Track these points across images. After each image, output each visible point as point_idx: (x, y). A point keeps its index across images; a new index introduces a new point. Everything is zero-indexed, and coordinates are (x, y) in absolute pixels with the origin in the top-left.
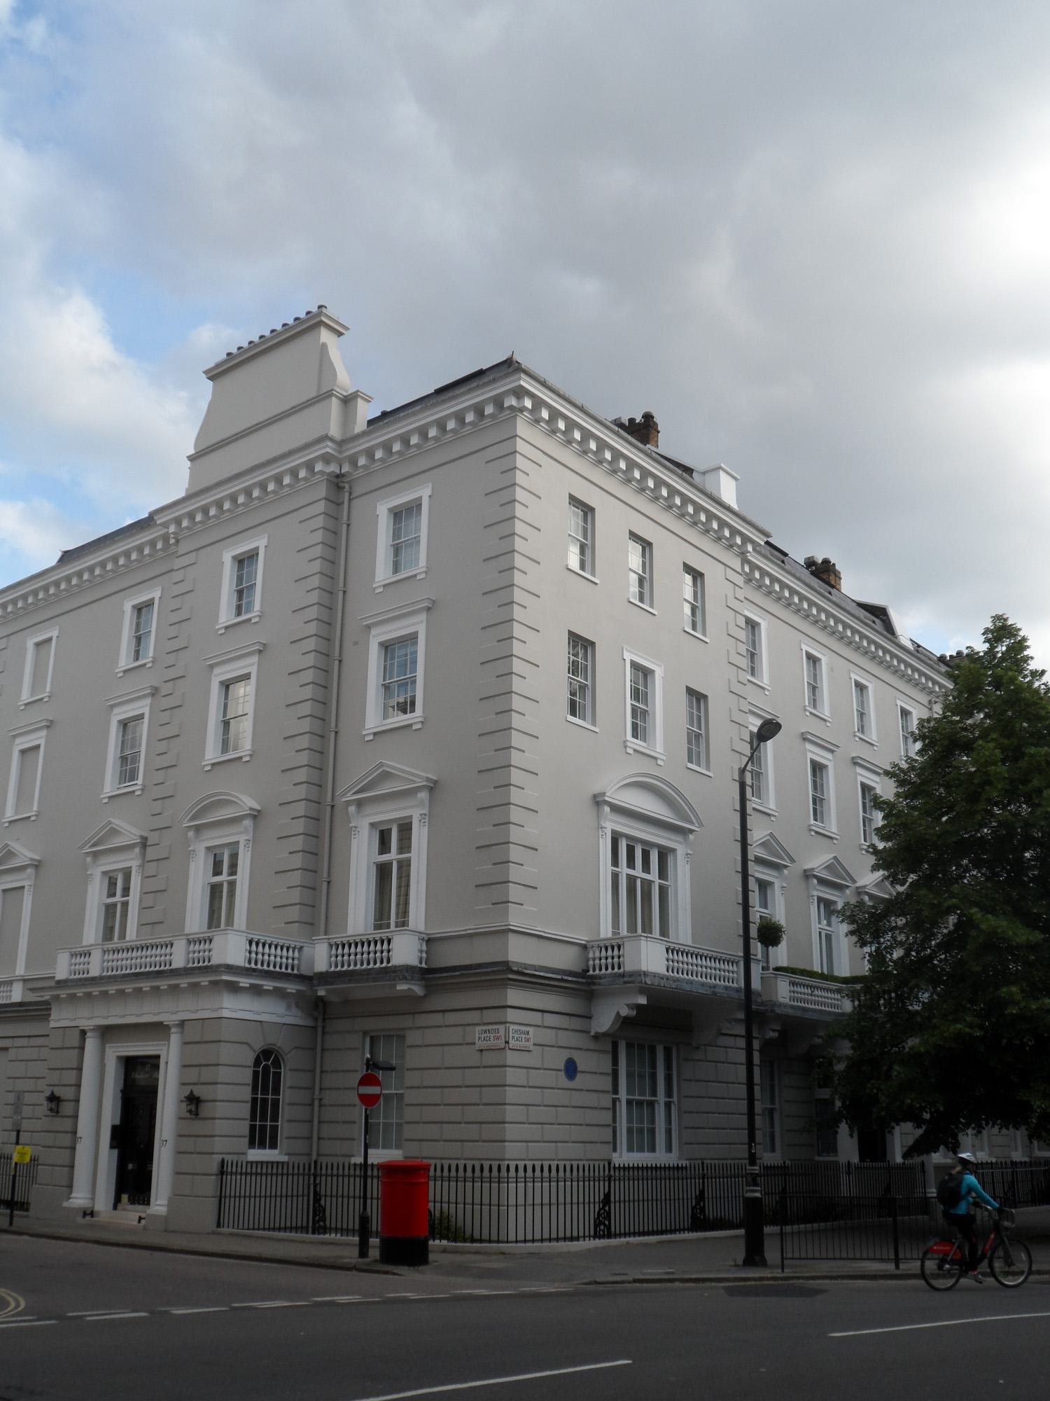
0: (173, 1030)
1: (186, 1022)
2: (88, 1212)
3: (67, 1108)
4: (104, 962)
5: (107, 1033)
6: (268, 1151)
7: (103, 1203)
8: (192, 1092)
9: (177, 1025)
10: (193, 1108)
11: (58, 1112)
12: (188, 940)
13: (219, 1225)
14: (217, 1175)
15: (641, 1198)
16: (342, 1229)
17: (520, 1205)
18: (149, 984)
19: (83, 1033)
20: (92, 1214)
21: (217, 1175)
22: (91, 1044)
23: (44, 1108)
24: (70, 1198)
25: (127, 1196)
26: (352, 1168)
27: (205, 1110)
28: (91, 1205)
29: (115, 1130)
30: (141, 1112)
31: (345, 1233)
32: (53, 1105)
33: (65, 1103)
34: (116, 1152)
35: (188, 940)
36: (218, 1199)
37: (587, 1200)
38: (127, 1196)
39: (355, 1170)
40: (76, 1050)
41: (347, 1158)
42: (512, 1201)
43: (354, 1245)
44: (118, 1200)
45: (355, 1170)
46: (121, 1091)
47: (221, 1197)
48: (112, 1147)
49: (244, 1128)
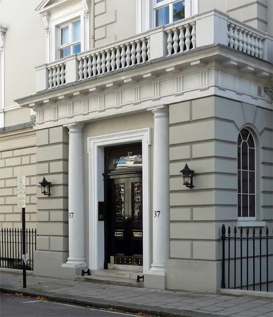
0: (156, 115)
1: (170, 106)
2: (86, 270)
3: (59, 191)
4: (48, 79)
5: (85, 127)
6: (249, 218)
7: (95, 261)
8: (187, 166)
9: (161, 110)
10: (46, 191)
11: (49, 194)
12: (165, 32)
13: (223, 286)
14: (218, 240)
15: (12, 241)
16: (261, 284)
17: (250, 257)
18: (111, 81)
19: (66, 130)
20: (89, 272)
21: (218, 240)
22: (73, 137)
23: (38, 191)
24: (67, 261)
25: (113, 257)
26: (238, 231)
27: (198, 182)
28: (85, 266)
29: (100, 204)
30: (122, 190)
31: (257, 287)
32: (188, 180)
33: (55, 188)
34: (103, 222)
35: (165, 32)
36: (220, 262)
37: (4, 241)
38: (113, 257)
39: (241, 232)
40: (61, 146)
41: (233, 223)
42: (20, 244)
43: (21, 274)
44: (107, 261)
45: (241, 232)
46: (103, 174)
47: (224, 260)
48: (99, 220)
49: (233, 198)
